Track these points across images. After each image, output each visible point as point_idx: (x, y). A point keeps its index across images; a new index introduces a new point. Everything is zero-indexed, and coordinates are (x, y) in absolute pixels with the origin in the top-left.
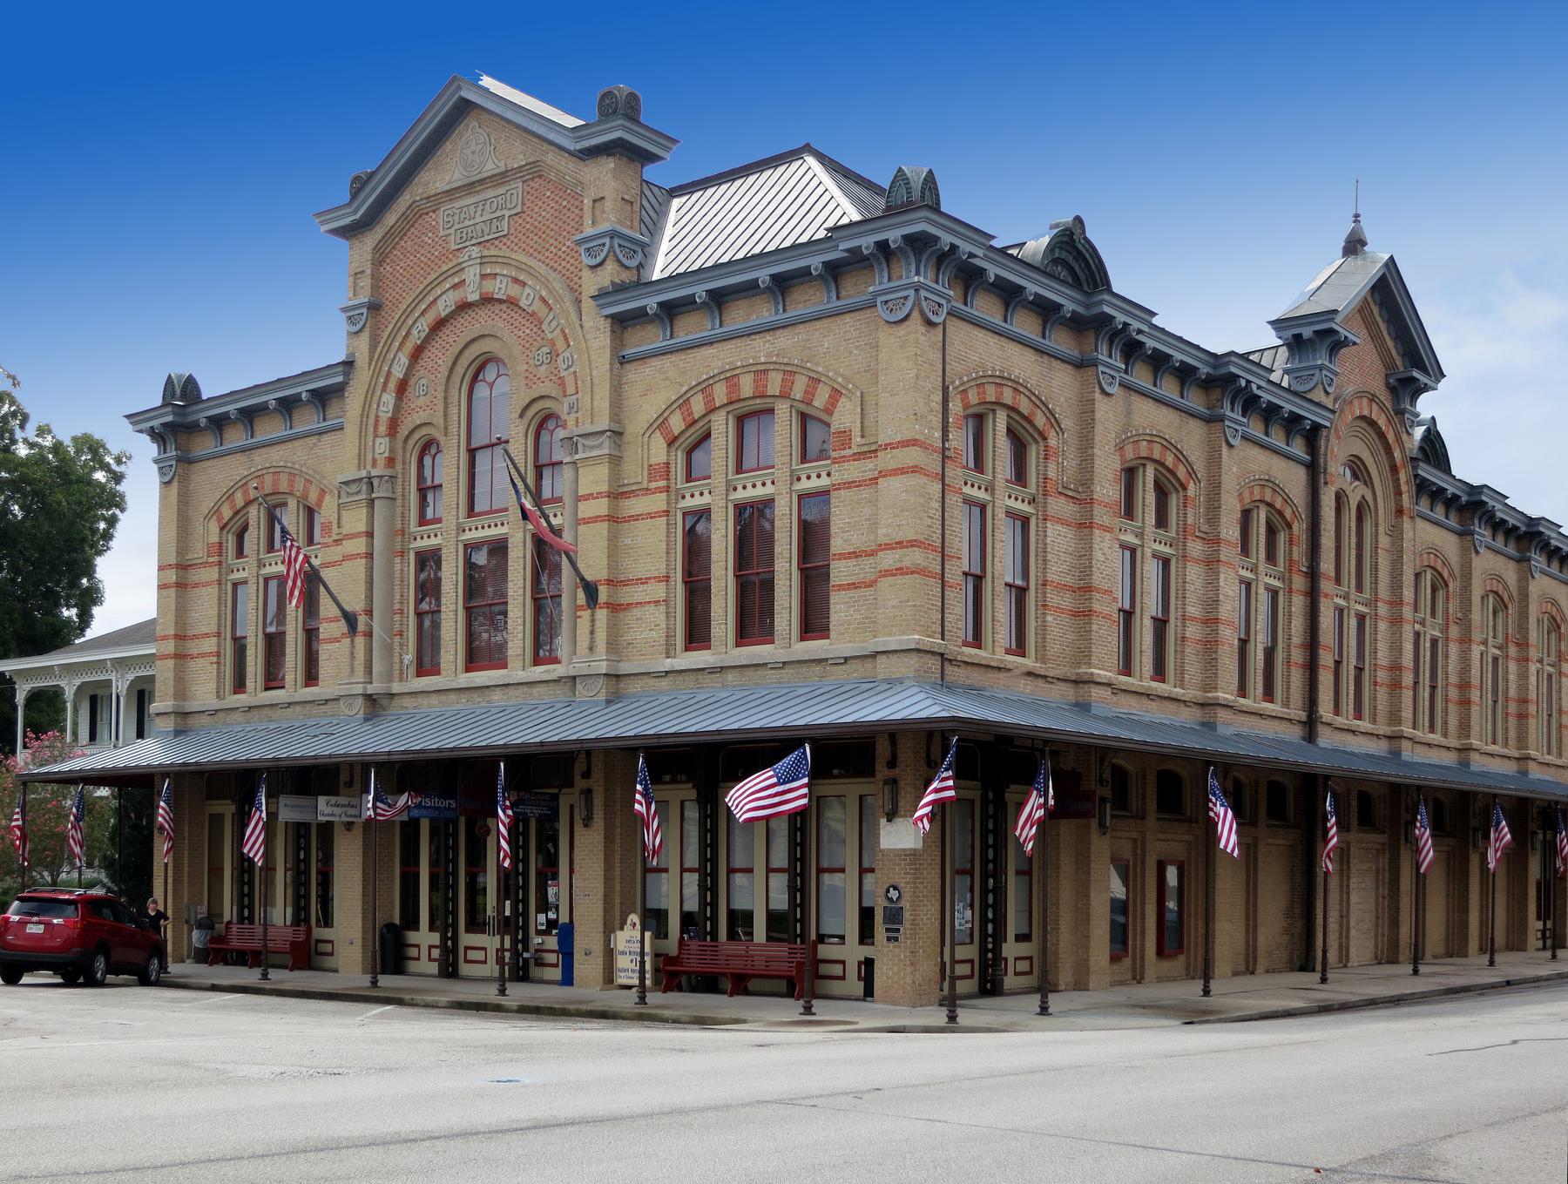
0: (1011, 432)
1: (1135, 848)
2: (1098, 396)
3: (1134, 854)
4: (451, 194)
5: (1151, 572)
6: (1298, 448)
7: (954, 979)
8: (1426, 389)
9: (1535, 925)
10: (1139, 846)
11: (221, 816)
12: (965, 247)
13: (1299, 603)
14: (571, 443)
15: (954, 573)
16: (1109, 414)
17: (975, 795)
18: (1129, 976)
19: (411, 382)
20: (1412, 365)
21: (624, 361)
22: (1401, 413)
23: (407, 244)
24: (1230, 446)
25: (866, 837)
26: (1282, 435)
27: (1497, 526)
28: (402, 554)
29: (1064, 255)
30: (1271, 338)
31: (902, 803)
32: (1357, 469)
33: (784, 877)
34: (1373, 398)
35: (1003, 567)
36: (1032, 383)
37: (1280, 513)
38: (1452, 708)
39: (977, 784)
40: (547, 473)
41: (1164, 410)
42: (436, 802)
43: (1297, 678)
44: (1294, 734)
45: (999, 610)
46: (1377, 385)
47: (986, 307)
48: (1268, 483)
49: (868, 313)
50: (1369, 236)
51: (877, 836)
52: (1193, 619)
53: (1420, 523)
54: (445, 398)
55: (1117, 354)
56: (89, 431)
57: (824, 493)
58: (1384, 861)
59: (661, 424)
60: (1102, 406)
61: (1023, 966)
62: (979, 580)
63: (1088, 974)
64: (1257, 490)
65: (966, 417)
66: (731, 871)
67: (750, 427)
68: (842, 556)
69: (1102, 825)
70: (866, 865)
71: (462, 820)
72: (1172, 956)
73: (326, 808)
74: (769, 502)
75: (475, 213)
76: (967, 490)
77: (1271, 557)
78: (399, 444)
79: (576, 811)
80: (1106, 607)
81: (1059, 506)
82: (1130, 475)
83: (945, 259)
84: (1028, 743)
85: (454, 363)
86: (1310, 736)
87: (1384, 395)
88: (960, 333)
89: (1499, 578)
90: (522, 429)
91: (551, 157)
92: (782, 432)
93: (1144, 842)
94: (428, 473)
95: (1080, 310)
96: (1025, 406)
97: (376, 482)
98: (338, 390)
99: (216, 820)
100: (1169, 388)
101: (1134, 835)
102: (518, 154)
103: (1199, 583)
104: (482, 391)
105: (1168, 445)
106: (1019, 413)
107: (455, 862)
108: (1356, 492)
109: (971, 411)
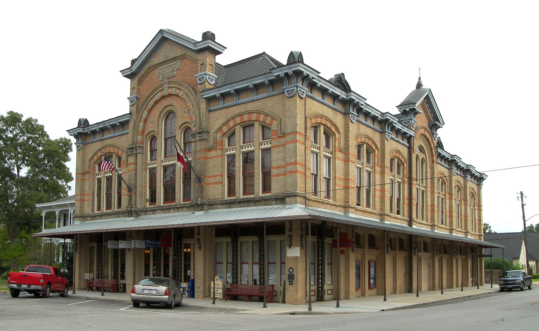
0: (325, 133)
1: (362, 257)
2: (350, 123)
3: (362, 259)
4: (160, 64)
5: (365, 175)
6: (405, 142)
7: (310, 297)
8: (439, 127)
9: (470, 279)
10: (363, 256)
11: (94, 247)
12: (311, 75)
13: (406, 186)
14: (193, 135)
15: (308, 173)
16: (353, 128)
17: (315, 240)
18: (360, 295)
19: (148, 119)
20: (435, 122)
21: (210, 111)
22: (433, 134)
23: (147, 79)
24: (387, 140)
25: (283, 253)
26: (401, 138)
27: (458, 167)
28: (145, 169)
29: (339, 84)
30: (397, 112)
31: (293, 242)
32: (421, 149)
33: (231, 265)
34: (425, 129)
35: (324, 172)
36: (331, 118)
37: (401, 161)
38: (448, 218)
39: (316, 237)
40: (187, 145)
41: (369, 128)
42: (154, 242)
43: (406, 208)
44: (405, 225)
45: (322, 186)
46: (426, 125)
47: (317, 95)
48: (398, 151)
49: (282, 95)
50: (423, 83)
51: (285, 253)
52: (377, 190)
53: (438, 165)
54: (158, 124)
55: (355, 111)
56: (12, 110)
57: (269, 149)
58: (431, 261)
59: (220, 129)
60: (351, 125)
61: (330, 292)
62: (316, 176)
63: (349, 294)
64: (394, 153)
65: (312, 127)
66: (242, 263)
67: (247, 130)
68: (274, 168)
69: (353, 250)
70: (282, 261)
71: (162, 248)
72: (373, 289)
73: (122, 245)
74: (253, 152)
75: (166, 70)
76: (312, 149)
77: (398, 173)
78: (145, 137)
79: (195, 245)
80: (353, 184)
81: (339, 155)
82: (359, 146)
83: (305, 78)
84: (331, 225)
85: (161, 113)
86: (410, 225)
87: (428, 128)
88: (309, 101)
89: (459, 182)
90: (180, 132)
91: (189, 53)
92: (257, 130)
93: (364, 254)
94: (153, 146)
95: (345, 97)
96: (329, 125)
97: (138, 148)
98: (127, 122)
99: (92, 249)
100: (369, 122)
101: (362, 253)
102: (179, 52)
103: (379, 179)
104: (169, 121)
105: (369, 138)
106: (327, 127)
107: (160, 261)
108: (421, 156)
109: (313, 125)
